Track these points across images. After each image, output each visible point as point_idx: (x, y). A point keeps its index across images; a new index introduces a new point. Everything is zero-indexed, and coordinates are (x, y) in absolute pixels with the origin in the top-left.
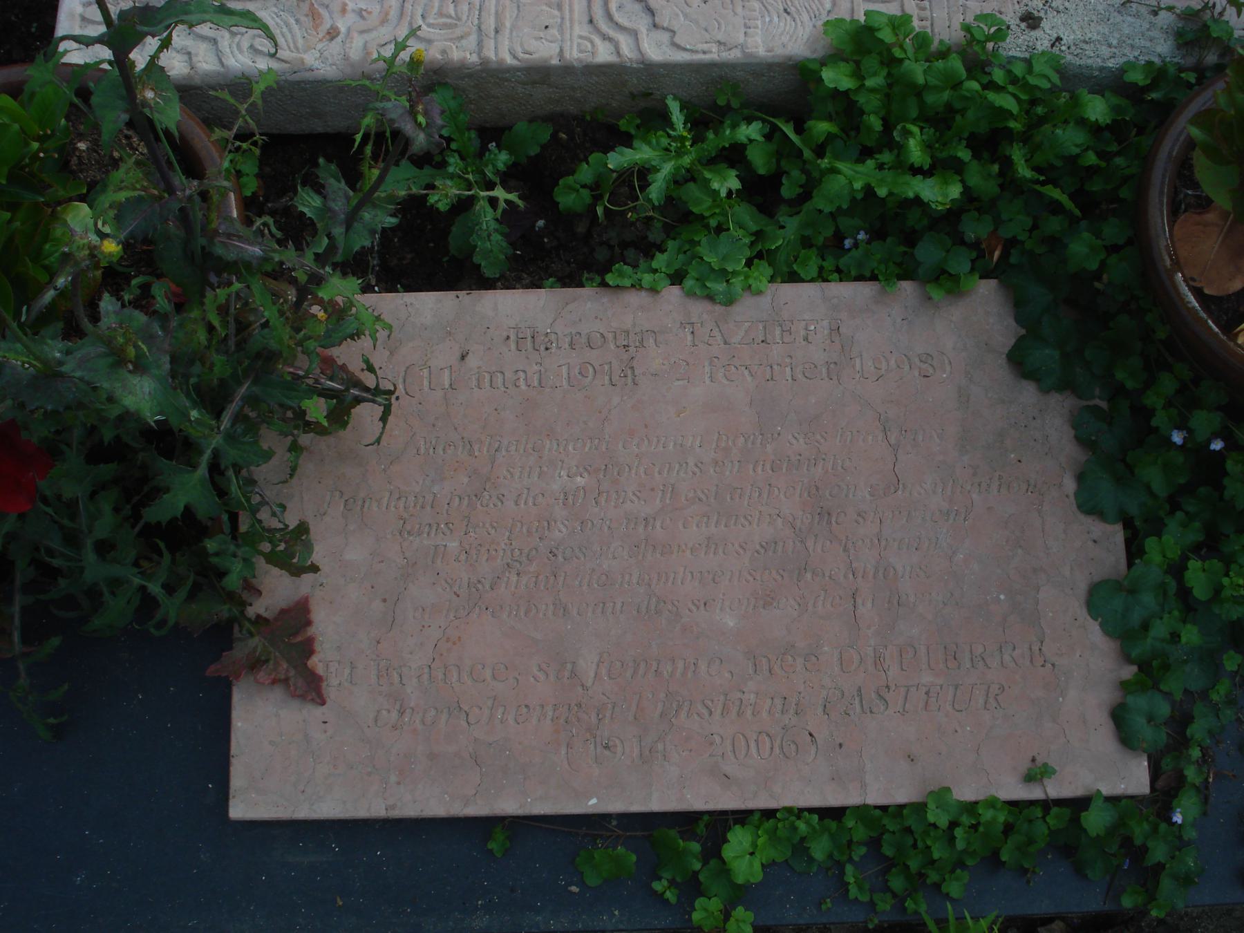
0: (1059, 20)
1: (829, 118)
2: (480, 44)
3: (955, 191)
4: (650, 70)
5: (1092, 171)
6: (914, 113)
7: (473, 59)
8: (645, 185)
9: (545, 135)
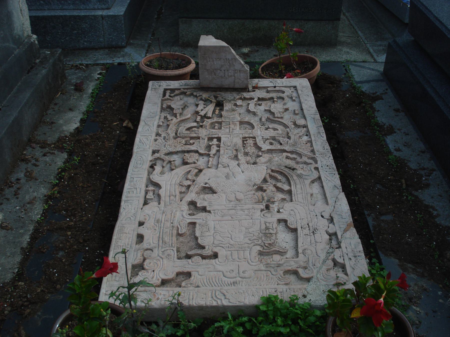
0: (310, 296)
1: (262, 317)
2: (189, 302)
3: (288, 330)
4: (224, 307)
5: (318, 326)
6: (279, 314)
7: (187, 304)
8: (223, 330)
9: (202, 321)
